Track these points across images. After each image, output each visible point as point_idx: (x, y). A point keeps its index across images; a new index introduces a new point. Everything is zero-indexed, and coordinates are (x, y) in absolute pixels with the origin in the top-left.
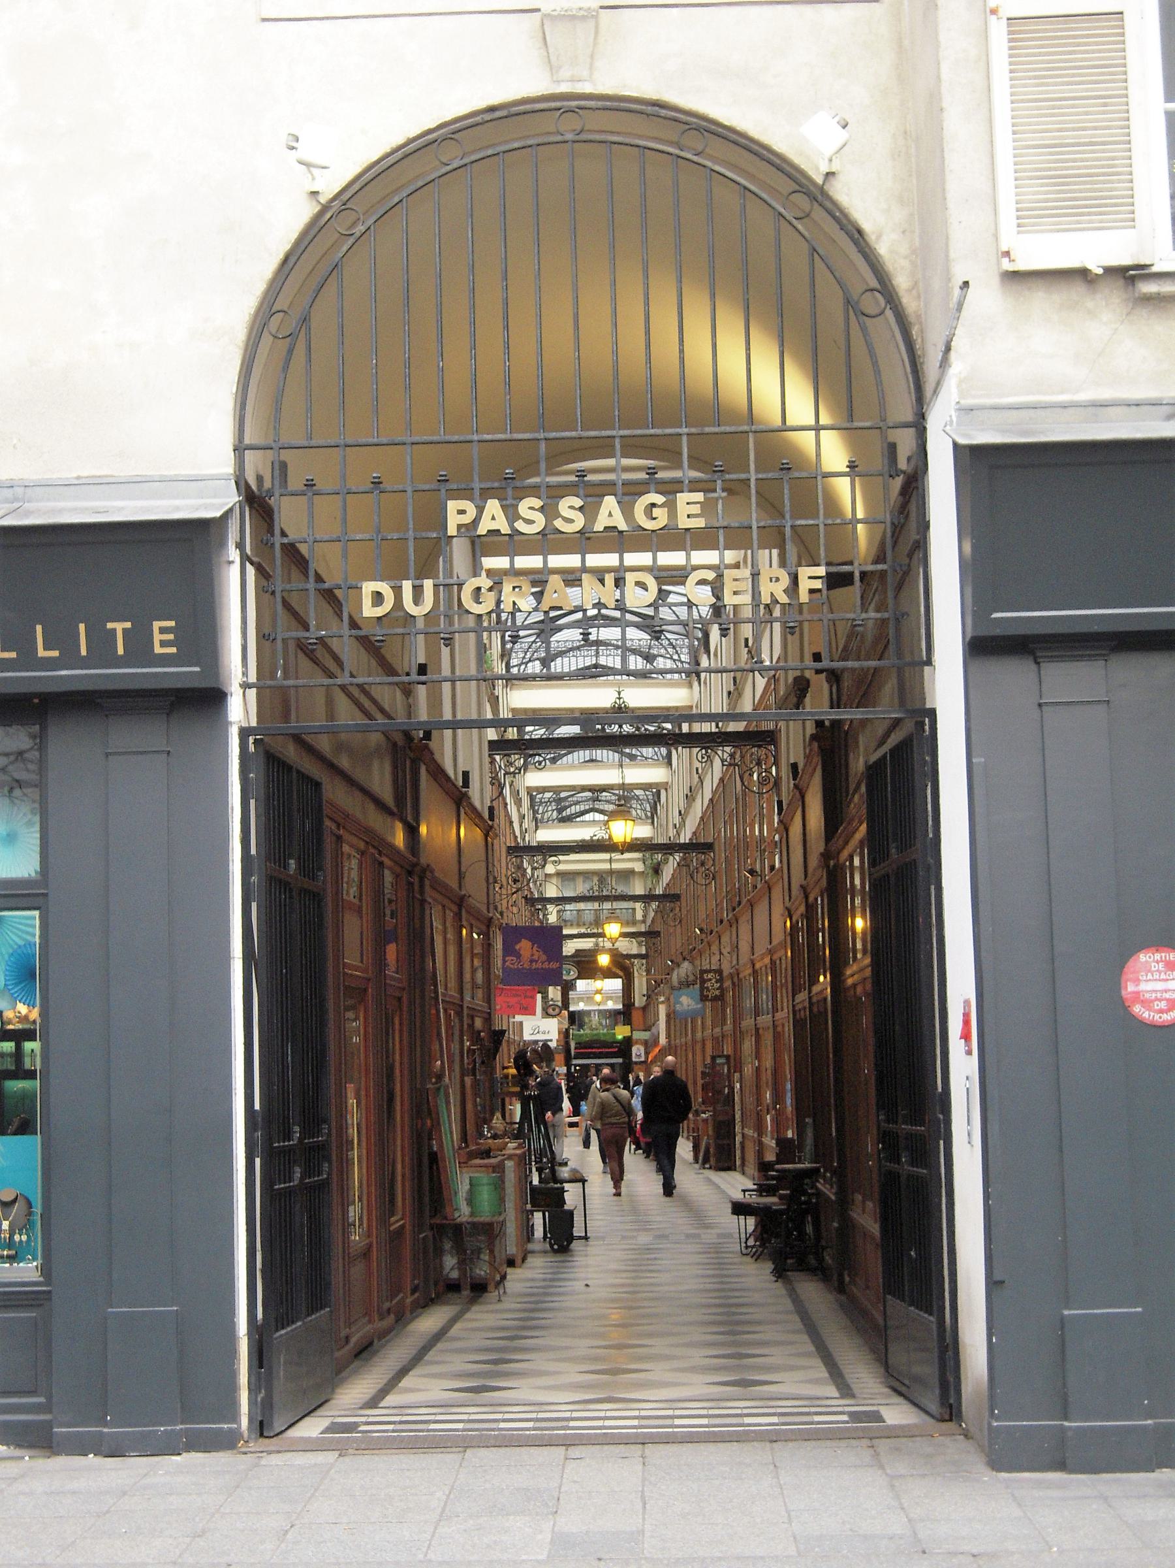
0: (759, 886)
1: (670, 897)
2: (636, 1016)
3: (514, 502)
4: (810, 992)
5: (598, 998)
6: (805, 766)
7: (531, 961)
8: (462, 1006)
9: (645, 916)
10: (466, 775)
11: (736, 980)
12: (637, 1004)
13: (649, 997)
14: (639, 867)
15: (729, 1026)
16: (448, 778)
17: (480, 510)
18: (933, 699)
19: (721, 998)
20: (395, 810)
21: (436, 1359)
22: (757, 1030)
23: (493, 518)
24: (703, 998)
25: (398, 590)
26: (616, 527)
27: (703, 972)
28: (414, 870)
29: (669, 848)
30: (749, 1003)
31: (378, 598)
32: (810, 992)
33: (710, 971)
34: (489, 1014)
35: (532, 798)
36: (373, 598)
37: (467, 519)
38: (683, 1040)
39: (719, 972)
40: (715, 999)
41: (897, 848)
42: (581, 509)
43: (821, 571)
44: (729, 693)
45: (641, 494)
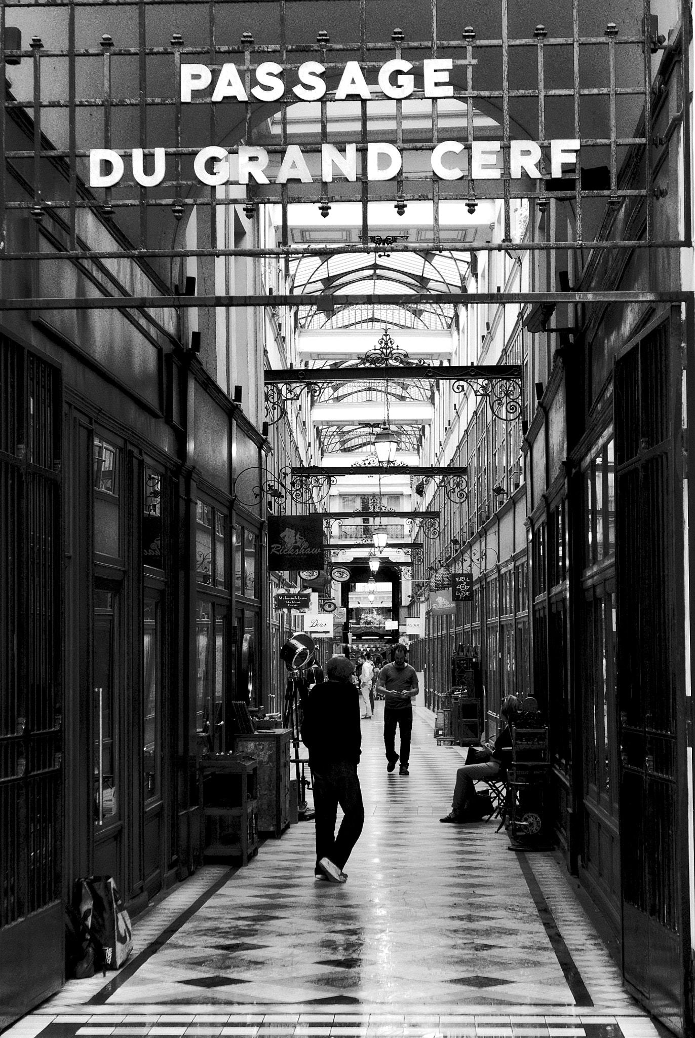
0: (505, 502)
1: (431, 515)
2: (403, 612)
3: (251, 67)
4: (549, 593)
5: (371, 597)
6: (549, 383)
7: (295, 548)
8: (231, 601)
9: (411, 531)
10: (238, 390)
11: (484, 583)
12: (403, 604)
13: (413, 597)
14: (407, 491)
15: (477, 623)
16: (219, 390)
17: (215, 75)
18: (691, 280)
19: (470, 598)
20: (160, 414)
21: (180, 943)
22: (502, 627)
23: (230, 84)
24: (455, 598)
25: (127, 159)
26: (359, 96)
27: (455, 576)
28: (181, 474)
29: (429, 472)
30: (494, 604)
31: (107, 167)
32: (549, 593)
33: (460, 575)
34: (260, 608)
35: (319, 432)
36: (103, 168)
37: (203, 83)
38: (440, 634)
39: (470, 576)
40: (466, 599)
41: (647, 442)
42: (322, 75)
43: (575, 144)
44: (483, 337)
45: (386, 60)
